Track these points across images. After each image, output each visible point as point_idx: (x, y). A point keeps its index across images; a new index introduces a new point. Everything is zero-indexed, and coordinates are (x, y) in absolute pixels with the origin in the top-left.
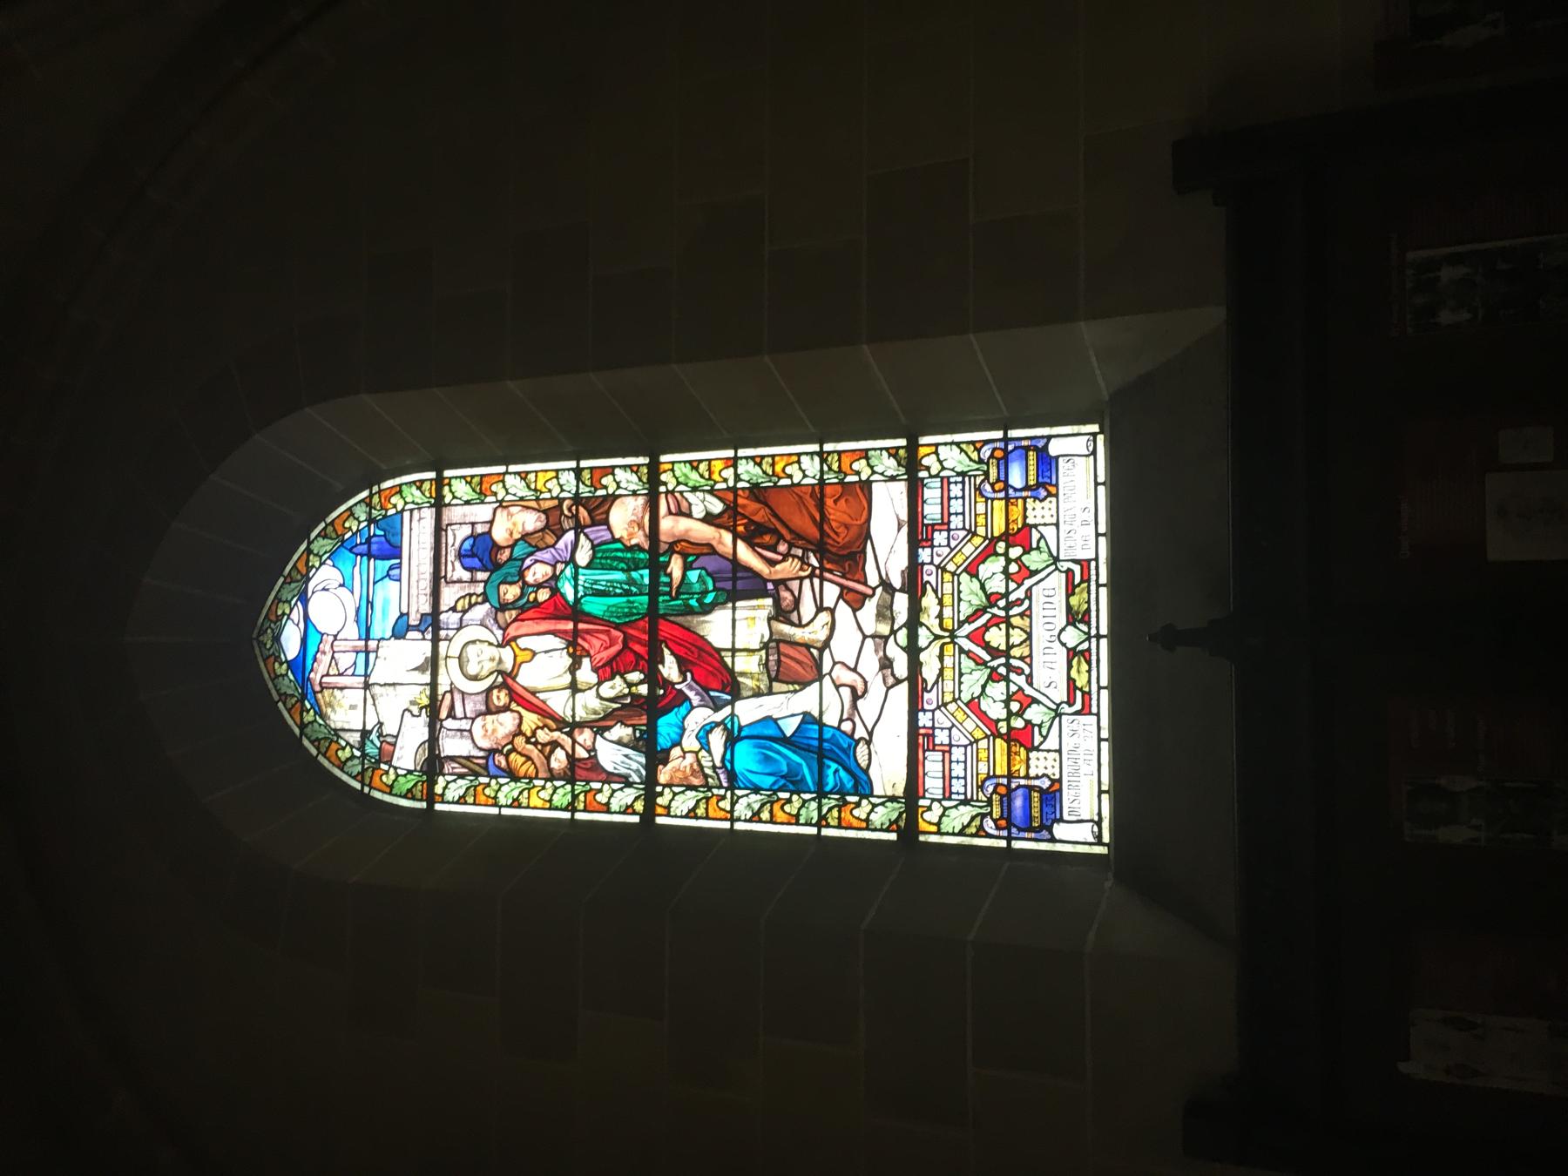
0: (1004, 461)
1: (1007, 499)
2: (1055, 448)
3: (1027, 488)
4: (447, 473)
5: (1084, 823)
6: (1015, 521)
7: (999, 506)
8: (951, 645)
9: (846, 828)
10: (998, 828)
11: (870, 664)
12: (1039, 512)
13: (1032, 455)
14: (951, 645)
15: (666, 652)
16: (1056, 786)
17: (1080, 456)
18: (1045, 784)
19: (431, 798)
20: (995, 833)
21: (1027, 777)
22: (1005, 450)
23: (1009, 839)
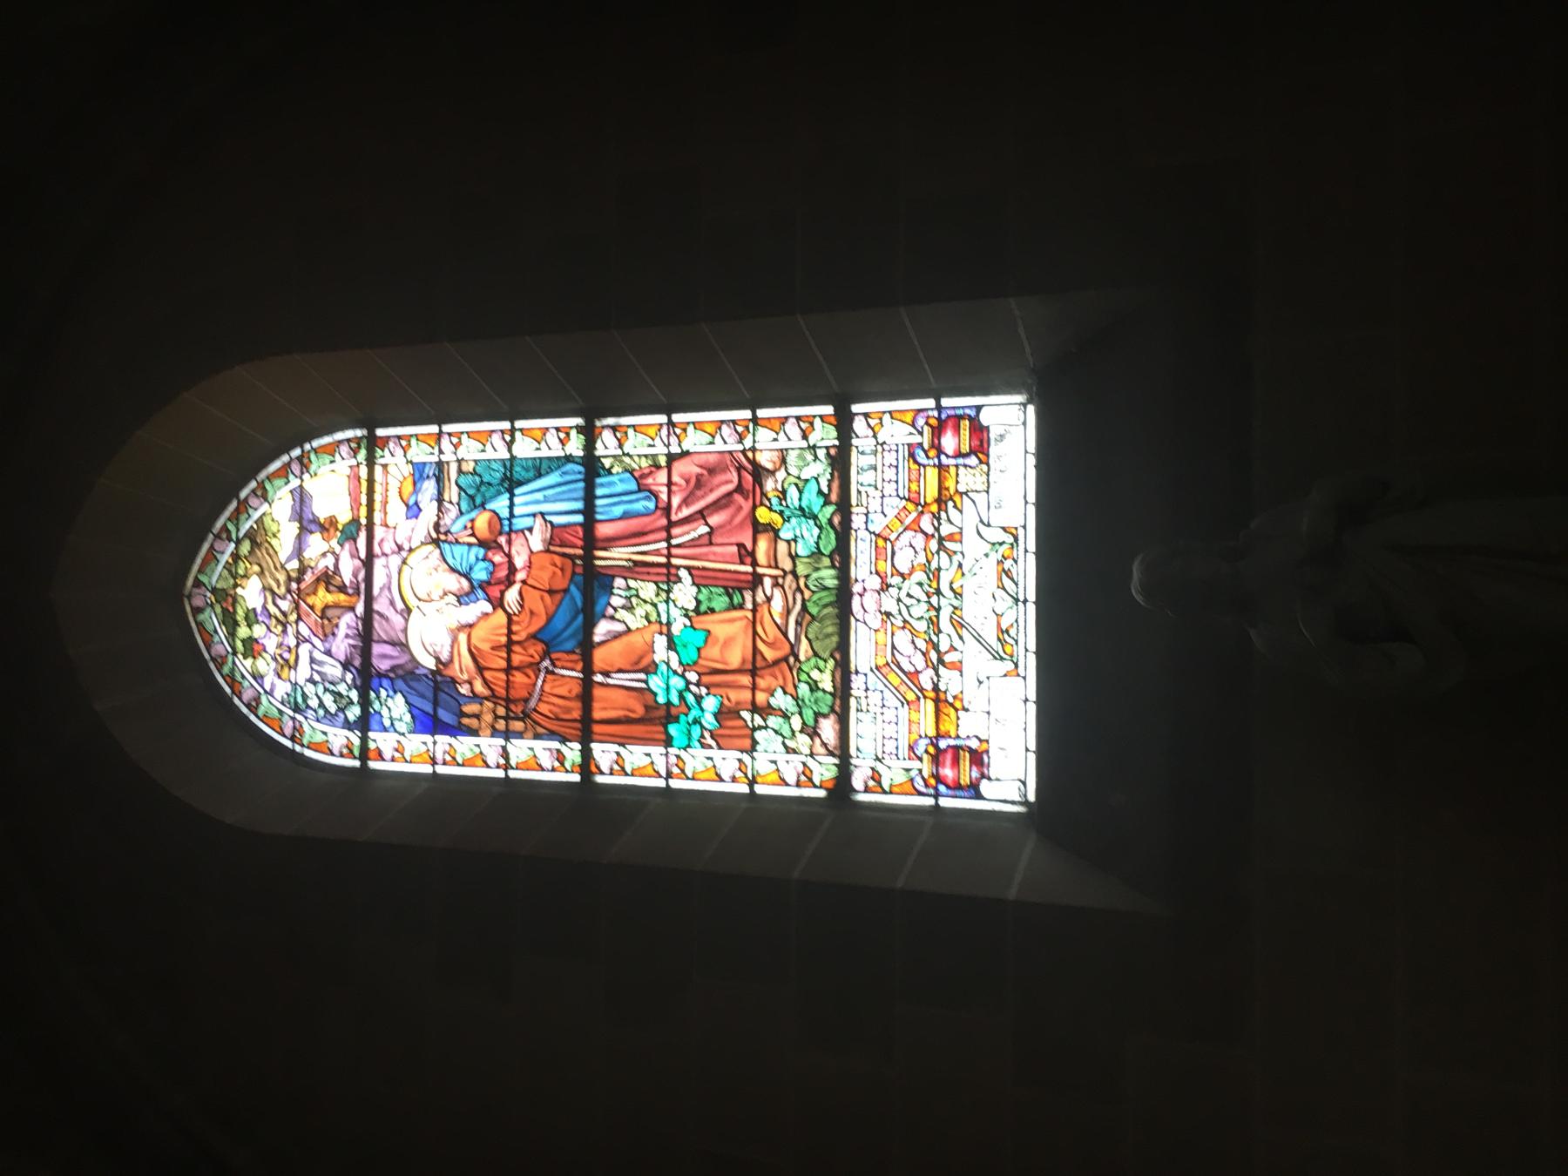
0: (938, 431)
1: (940, 467)
2: (985, 418)
3: (959, 455)
4: (380, 432)
5: (1011, 780)
6: (568, 710)
7: (932, 474)
8: (889, 605)
9: (719, 500)
10: (927, 785)
11: (920, 662)
12: (968, 478)
13: (965, 424)
14: (889, 605)
15: (1139, 598)
16: (985, 746)
17: (1011, 420)
18: (974, 744)
19: (364, 754)
20: (923, 790)
21: (958, 737)
22: (939, 419)
23: (937, 795)
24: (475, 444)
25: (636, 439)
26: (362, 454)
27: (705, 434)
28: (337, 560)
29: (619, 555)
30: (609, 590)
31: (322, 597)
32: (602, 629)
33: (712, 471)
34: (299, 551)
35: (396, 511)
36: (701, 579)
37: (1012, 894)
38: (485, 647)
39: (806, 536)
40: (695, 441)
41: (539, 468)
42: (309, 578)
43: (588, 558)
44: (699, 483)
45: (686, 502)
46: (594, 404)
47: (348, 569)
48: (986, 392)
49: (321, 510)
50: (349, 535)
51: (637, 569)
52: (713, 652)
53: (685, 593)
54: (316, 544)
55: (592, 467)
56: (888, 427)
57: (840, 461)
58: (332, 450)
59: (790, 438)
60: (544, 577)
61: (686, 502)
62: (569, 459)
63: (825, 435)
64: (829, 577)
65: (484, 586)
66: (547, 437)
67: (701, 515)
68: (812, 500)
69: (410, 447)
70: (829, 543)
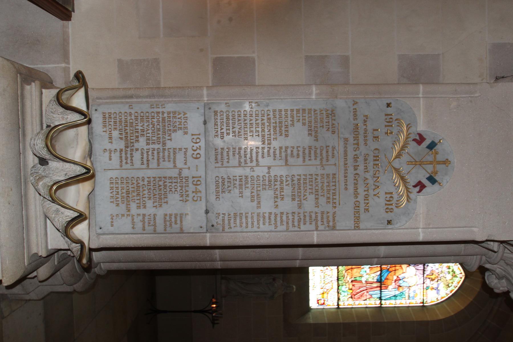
8: (214, 306)
12: (320, 297)
14: (214, 306)
17: (313, 304)
24: (402, 302)
25: (373, 303)
26: (425, 301)
27: (360, 303)
28: (508, 280)
29: (375, 285)
30: (377, 280)
31: (433, 277)
32: (379, 273)
33: (359, 298)
34: (438, 285)
35: (418, 292)
36: (361, 282)
37: (297, 266)
38: (400, 270)
39: (343, 288)
40: (363, 302)
41: (390, 298)
42: (436, 280)
43: (381, 284)
44: (361, 296)
45: (364, 293)
46: (380, 309)
47: (428, 281)
48: (317, 309)
49: (434, 291)
50: (427, 288)
51: (372, 283)
52: (359, 271)
53: (363, 280)
54: (435, 285)
55: (380, 298)
56: (331, 303)
57: (339, 299)
58: (432, 302)
59: (347, 302)
60: (389, 281)
61: (364, 293)
62: (385, 300)
63: (340, 303)
64: (340, 282)
65: (400, 280)
66: (386, 304)
67: (361, 291)
68: (342, 293)
69: (416, 302)
70: (340, 287)
